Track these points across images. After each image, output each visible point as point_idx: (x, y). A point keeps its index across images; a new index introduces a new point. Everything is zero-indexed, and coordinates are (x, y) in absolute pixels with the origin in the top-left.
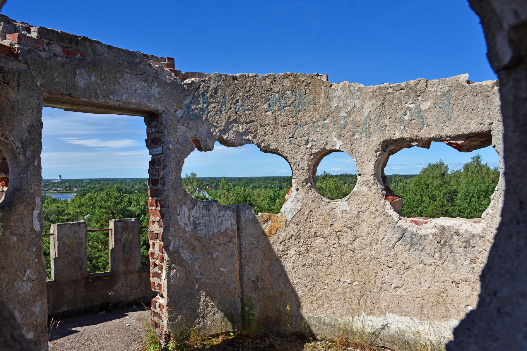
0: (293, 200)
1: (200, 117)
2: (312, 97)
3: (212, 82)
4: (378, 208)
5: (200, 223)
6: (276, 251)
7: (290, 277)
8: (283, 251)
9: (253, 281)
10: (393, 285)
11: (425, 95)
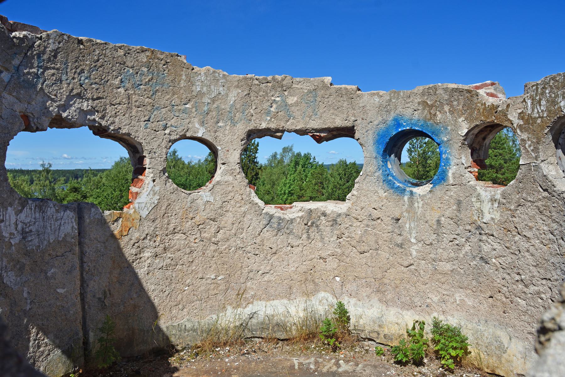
0: (149, 193)
1: (34, 85)
2: (171, 78)
3: (51, 41)
4: (244, 197)
5: (31, 231)
6: (127, 256)
7: (144, 284)
8: (136, 255)
9: (99, 299)
10: (260, 272)
11: (291, 90)
